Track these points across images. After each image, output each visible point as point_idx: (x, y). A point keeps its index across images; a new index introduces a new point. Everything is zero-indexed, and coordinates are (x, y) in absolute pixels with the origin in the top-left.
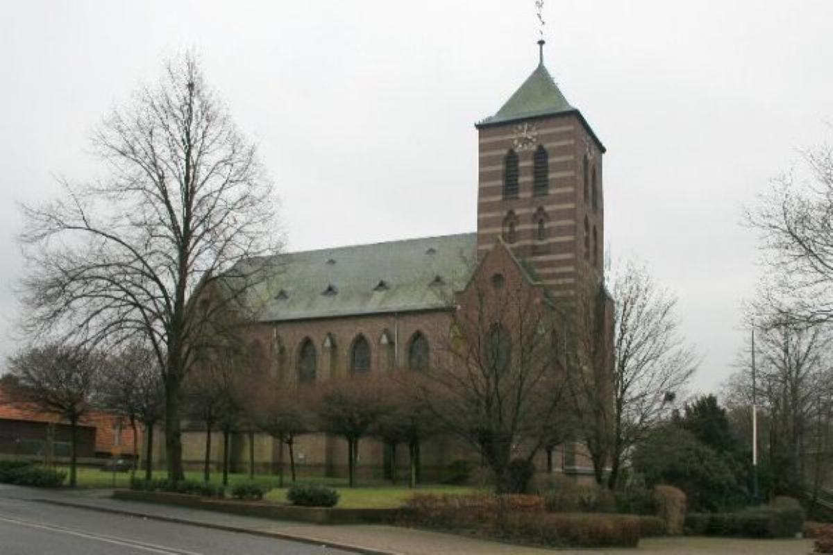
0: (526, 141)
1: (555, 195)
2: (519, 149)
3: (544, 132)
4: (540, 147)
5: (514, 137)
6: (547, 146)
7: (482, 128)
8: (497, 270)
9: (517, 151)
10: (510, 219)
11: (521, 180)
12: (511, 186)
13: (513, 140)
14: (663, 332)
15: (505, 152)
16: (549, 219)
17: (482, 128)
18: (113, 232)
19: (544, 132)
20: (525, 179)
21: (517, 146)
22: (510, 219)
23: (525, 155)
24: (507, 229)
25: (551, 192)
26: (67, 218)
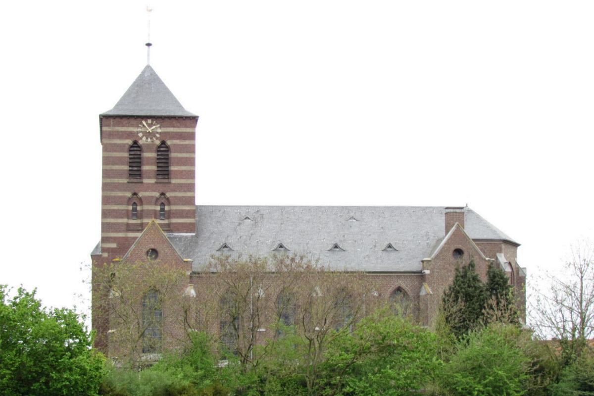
0: (148, 135)
1: (155, 191)
2: (143, 141)
3: (171, 130)
4: (163, 143)
5: (139, 130)
6: (169, 143)
7: (105, 119)
8: (161, 254)
9: (141, 142)
10: (136, 200)
11: (145, 168)
12: (135, 171)
13: (138, 133)
14: (419, 359)
15: (130, 142)
16: (169, 204)
17: (105, 119)
18: (564, 311)
19: (171, 130)
20: (149, 168)
21: (141, 138)
22: (136, 200)
23: (149, 148)
24: (167, 208)
25: (173, 181)
26: (379, 289)
